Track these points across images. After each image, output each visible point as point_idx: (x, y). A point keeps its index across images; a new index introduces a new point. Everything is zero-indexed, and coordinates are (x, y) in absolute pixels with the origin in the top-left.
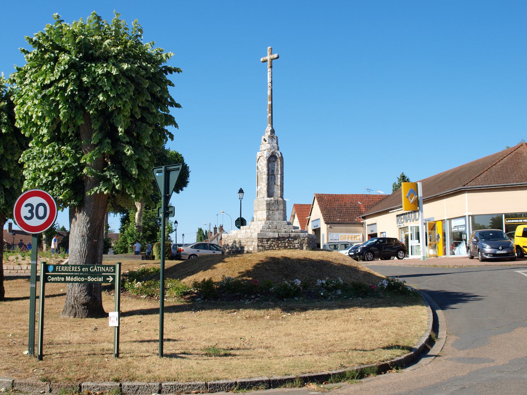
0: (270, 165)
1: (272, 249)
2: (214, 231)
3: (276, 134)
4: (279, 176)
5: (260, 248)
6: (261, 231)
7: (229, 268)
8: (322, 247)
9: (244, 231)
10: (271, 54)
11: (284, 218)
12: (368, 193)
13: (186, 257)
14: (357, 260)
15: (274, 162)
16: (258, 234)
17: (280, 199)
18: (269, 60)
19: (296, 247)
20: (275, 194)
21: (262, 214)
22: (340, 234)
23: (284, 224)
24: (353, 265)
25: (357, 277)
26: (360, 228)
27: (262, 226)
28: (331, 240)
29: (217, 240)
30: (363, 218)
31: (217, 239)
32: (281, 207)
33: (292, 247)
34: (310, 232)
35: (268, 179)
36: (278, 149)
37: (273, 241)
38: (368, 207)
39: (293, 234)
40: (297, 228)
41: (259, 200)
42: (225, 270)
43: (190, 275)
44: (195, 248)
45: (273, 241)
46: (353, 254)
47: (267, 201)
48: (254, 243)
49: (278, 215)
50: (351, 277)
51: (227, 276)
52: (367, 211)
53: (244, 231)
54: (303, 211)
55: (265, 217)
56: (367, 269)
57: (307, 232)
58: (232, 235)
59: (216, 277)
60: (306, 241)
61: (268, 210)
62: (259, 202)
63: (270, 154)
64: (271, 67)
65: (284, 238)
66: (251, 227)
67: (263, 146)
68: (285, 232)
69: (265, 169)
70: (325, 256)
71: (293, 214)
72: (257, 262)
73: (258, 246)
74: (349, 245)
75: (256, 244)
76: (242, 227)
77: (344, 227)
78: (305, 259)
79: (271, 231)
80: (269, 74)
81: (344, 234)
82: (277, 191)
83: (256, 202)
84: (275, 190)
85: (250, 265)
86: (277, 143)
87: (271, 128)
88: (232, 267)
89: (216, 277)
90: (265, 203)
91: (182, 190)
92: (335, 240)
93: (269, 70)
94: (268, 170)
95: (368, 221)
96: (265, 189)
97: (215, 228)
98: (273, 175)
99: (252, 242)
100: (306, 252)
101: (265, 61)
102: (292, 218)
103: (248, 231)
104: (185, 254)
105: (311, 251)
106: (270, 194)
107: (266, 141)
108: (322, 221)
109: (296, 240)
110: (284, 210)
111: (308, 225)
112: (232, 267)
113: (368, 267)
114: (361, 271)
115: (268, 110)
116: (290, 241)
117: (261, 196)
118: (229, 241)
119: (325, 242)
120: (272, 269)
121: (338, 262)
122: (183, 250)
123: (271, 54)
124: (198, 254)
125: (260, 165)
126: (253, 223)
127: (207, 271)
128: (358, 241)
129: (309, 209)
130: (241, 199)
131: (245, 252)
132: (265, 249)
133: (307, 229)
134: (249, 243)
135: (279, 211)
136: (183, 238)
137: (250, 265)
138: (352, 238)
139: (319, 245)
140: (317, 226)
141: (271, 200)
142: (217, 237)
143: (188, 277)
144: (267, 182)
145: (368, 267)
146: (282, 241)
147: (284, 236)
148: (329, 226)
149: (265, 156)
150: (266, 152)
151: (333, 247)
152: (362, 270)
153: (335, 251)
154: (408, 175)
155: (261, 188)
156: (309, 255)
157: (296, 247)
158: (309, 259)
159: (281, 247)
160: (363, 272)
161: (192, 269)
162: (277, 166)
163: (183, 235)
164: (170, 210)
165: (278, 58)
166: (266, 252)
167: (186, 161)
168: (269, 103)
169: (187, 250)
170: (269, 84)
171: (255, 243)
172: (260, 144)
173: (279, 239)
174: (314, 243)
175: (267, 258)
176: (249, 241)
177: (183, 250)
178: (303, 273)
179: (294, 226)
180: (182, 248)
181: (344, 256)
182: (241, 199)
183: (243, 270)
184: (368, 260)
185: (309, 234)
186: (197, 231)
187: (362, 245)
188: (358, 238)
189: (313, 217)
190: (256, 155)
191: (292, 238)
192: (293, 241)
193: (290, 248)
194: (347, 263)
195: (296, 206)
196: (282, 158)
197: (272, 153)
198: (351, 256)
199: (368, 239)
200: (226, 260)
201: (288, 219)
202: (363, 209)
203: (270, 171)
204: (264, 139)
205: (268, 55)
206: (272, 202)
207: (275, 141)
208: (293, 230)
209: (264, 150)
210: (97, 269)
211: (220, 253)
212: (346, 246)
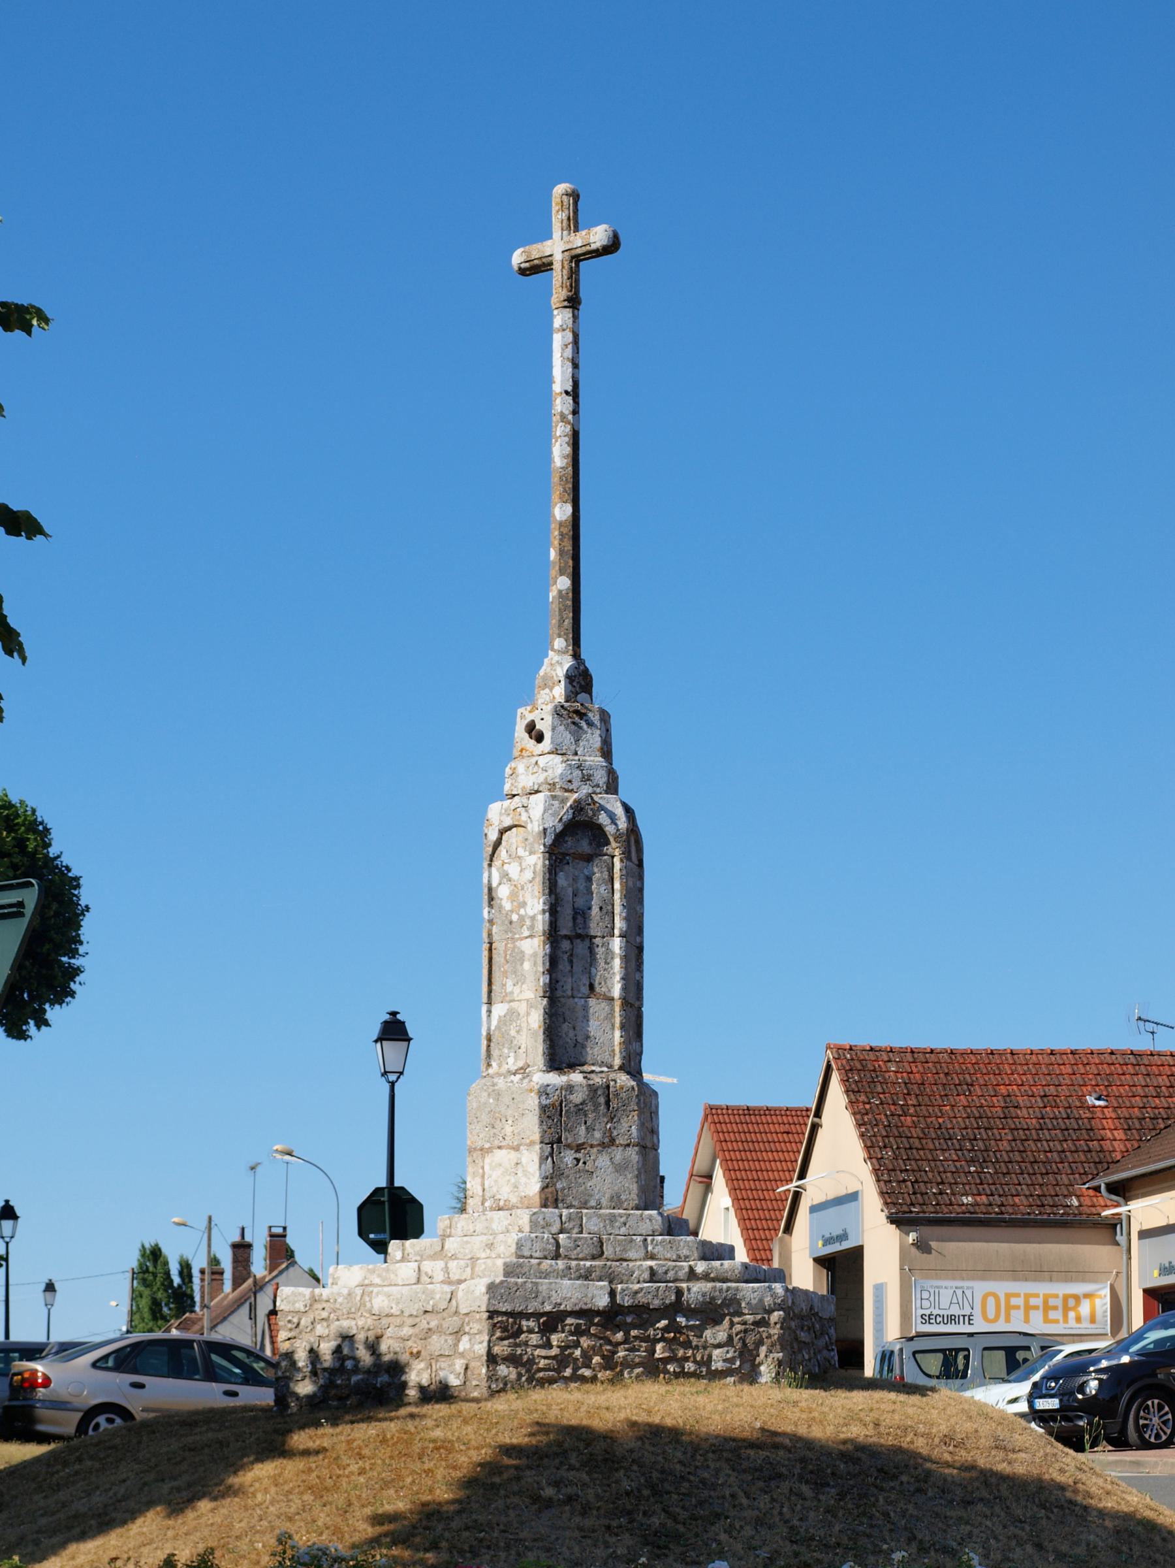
0: (562, 881)
1: (575, 1378)
2: (236, 1261)
3: (602, 695)
4: (617, 944)
5: (503, 1370)
6: (509, 1271)
7: (319, 1491)
8: (870, 1369)
9: (407, 1271)
10: (574, 224)
11: (643, 1190)
12: (1142, 1043)
13: (68, 1424)
14: (1079, 1448)
15: (589, 859)
16: (491, 1288)
17: (623, 1079)
18: (558, 257)
19: (718, 1365)
20: (593, 1052)
21: (512, 1171)
22: (980, 1288)
23: (645, 1228)
24: (1053, 1474)
25: (1080, 1551)
26: (1096, 1253)
27: (513, 1237)
28: (927, 1319)
29: (253, 1316)
30: (1114, 1188)
31: (253, 1309)
32: (629, 1127)
33: (690, 1366)
34: (804, 1276)
35: (553, 963)
36: (612, 787)
37: (578, 1332)
38: (1146, 1128)
39: (696, 1291)
40: (723, 1252)
41: (501, 1083)
42: (296, 1504)
43: (83, 1536)
44: (118, 1368)
45: (578, 1332)
46: (1053, 1404)
47: (543, 1091)
48: (464, 1344)
49: (608, 1175)
50: (1039, 1546)
51: (304, 1539)
52: (1135, 1150)
53: (407, 1271)
54: (762, 1148)
55: (533, 1186)
56: (1134, 1501)
57: (780, 1276)
58: (347, 1295)
59: (243, 1545)
60: (775, 1331)
61: (553, 1142)
62: (498, 1095)
63: (564, 811)
64: (573, 302)
65: (643, 1314)
66: (451, 1245)
67: (521, 766)
68: (653, 1276)
69: (535, 905)
70: (887, 1420)
71: (701, 1166)
72: (485, 1454)
73: (492, 1359)
74: (1035, 1352)
75: (481, 1349)
76: (394, 1246)
77: (1004, 1247)
78: (770, 1442)
79: (566, 1273)
80: (559, 342)
81: (1001, 1288)
82: (605, 1034)
83: (478, 1095)
84: (594, 1027)
85: (440, 1473)
86: (606, 752)
87: (568, 662)
88: (336, 1488)
89: (243, 1545)
90: (533, 1102)
91: (42, 1022)
92: (952, 1319)
93: (561, 318)
94: (553, 910)
95: (1146, 1211)
96: (535, 1019)
97: (242, 1249)
98: (583, 936)
99: (458, 1333)
100: (776, 1394)
101: (540, 267)
102: (696, 1189)
103: (433, 1267)
104: (60, 1405)
105: (806, 1394)
106: (562, 1049)
107: (539, 738)
108: (873, 1207)
109: (717, 1321)
110: (648, 1146)
111: (788, 1229)
112: (336, 1488)
113: (1141, 1484)
114: (1102, 1513)
115: (553, 554)
116: (678, 1329)
117: (512, 1063)
118: (320, 1329)
119: (893, 1332)
120: (570, 1499)
121: (963, 1456)
122: (47, 1382)
123: (574, 224)
124: (136, 1403)
125: (505, 876)
126: (462, 1222)
127: (190, 1515)
128: (1085, 1327)
129: (797, 1131)
130: (392, 1077)
131: (412, 1393)
132: (532, 1376)
133: (786, 1257)
134: (437, 1343)
135: (618, 1154)
136: (49, 1305)
137: (440, 1473)
138: (1047, 1308)
139: (852, 1354)
140: (843, 1237)
141: (570, 1088)
142: (248, 1300)
143: (72, 1548)
144: (544, 980)
145: (1141, 1484)
146: (637, 1330)
147: (642, 1299)
148: (912, 1237)
149: (535, 827)
150: (538, 803)
151: (934, 1364)
152: (1109, 1504)
153: (946, 1392)
155: (512, 1015)
156: (793, 1414)
157: (718, 1365)
158: (796, 1438)
159: (628, 1365)
160: (1115, 1515)
161: (98, 1499)
162: (607, 887)
163: (50, 1287)
165: (612, 247)
166: (537, 1396)
167: (65, 847)
168: (562, 512)
169: (69, 1382)
170: (562, 405)
171: (475, 1344)
172: (506, 753)
173: (612, 1316)
174: (824, 1341)
175: (541, 1427)
176: (439, 1330)
177: (47, 1382)
178: (759, 1522)
179: (705, 1244)
180: (39, 1367)
181: (1003, 1416)
182: (392, 1077)
183: (401, 1506)
184: (1146, 1445)
185: (795, 1292)
186: (133, 1260)
187: (1109, 1353)
188: (1085, 1309)
189: (818, 1186)
190: (481, 817)
191: (690, 1312)
192: (699, 1331)
193: (681, 1374)
194: (1021, 1465)
195: (716, 1116)
196: (633, 840)
197: (578, 807)
198: (1036, 1415)
199: (1147, 1316)
200: (300, 1439)
201: (673, 1198)
202: (1116, 1140)
203: (566, 913)
204: (531, 728)
205: (557, 234)
206: (577, 1098)
207: (593, 738)
208: (701, 1267)
209: (531, 789)
211: (264, 1396)
212: (1013, 1358)
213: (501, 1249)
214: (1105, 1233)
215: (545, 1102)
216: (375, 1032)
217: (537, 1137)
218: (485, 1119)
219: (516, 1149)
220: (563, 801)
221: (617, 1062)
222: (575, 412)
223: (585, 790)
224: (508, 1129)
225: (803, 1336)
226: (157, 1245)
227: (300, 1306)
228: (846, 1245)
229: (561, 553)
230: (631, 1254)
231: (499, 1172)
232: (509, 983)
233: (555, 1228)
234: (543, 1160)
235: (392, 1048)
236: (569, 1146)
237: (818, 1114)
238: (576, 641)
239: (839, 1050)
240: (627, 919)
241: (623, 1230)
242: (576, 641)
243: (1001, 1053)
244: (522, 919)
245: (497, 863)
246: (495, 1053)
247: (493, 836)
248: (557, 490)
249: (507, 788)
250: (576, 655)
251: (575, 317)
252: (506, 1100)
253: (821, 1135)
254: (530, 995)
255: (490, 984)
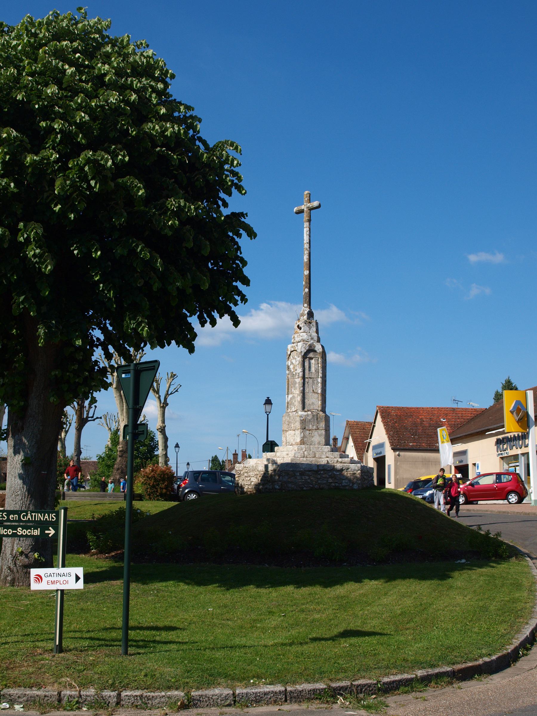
2: (234, 458)
12: (454, 406)
27: (293, 452)
32: (322, 425)
36: (319, 341)
55: (298, 440)
61: (304, 429)
71: (346, 435)
80: (306, 230)
86: (317, 332)
87: (308, 310)
90: (298, 419)
93: (306, 224)
101: (301, 212)
102: (345, 441)
107: (300, 329)
111: (367, 451)
117: (293, 409)
125: (292, 363)
130: (268, 413)
135: (320, 432)
140: (381, 453)
141: (308, 415)
148: (397, 453)
154: (515, 382)
155: (294, 397)
164: (141, 429)
165: (319, 207)
168: (306, 272)
170: (306, 246)
182: (268, 413)
197: (310, 346)
206: (310, 418)
210: (32, 516)
213: (290, 455)
214: (145, 377)
215: (301, 419)
216: (264, 402)
217: (299, 428)
218: (287, 423)
219: (294, 430)
220: (306, 344)
221: (320, 409)
222: (310, 248)
223: (312, 341)
224: (292, 426)
225: (365, 477)
226: (216, 456)
227: (241, 469)
228: (381, 455)
229: (306, 283)
230: (323, 457)
231: (290, 436)
232: (293, 390)
233: (304, 450)
234: (301, 433)
235: (268, 407)
236: (307, 430)
237: (375, 423)
238: (310, 305)
239: (380, 408)
240: (322, 374)
241: (321, 451)
242: (310, 305)
243: (420, 408)
244: (296, 373)
245: (290, 360)
246: (289, 407)
247: (289, 353)
248: (306, 267)
249: (292, 341)
250: (310, 308)
251: (310, 224)
252: (292, 418)
253: (375, 428)
254: (298, 392)
255: (288, 390)
